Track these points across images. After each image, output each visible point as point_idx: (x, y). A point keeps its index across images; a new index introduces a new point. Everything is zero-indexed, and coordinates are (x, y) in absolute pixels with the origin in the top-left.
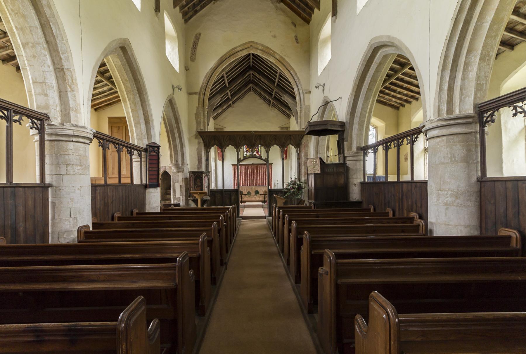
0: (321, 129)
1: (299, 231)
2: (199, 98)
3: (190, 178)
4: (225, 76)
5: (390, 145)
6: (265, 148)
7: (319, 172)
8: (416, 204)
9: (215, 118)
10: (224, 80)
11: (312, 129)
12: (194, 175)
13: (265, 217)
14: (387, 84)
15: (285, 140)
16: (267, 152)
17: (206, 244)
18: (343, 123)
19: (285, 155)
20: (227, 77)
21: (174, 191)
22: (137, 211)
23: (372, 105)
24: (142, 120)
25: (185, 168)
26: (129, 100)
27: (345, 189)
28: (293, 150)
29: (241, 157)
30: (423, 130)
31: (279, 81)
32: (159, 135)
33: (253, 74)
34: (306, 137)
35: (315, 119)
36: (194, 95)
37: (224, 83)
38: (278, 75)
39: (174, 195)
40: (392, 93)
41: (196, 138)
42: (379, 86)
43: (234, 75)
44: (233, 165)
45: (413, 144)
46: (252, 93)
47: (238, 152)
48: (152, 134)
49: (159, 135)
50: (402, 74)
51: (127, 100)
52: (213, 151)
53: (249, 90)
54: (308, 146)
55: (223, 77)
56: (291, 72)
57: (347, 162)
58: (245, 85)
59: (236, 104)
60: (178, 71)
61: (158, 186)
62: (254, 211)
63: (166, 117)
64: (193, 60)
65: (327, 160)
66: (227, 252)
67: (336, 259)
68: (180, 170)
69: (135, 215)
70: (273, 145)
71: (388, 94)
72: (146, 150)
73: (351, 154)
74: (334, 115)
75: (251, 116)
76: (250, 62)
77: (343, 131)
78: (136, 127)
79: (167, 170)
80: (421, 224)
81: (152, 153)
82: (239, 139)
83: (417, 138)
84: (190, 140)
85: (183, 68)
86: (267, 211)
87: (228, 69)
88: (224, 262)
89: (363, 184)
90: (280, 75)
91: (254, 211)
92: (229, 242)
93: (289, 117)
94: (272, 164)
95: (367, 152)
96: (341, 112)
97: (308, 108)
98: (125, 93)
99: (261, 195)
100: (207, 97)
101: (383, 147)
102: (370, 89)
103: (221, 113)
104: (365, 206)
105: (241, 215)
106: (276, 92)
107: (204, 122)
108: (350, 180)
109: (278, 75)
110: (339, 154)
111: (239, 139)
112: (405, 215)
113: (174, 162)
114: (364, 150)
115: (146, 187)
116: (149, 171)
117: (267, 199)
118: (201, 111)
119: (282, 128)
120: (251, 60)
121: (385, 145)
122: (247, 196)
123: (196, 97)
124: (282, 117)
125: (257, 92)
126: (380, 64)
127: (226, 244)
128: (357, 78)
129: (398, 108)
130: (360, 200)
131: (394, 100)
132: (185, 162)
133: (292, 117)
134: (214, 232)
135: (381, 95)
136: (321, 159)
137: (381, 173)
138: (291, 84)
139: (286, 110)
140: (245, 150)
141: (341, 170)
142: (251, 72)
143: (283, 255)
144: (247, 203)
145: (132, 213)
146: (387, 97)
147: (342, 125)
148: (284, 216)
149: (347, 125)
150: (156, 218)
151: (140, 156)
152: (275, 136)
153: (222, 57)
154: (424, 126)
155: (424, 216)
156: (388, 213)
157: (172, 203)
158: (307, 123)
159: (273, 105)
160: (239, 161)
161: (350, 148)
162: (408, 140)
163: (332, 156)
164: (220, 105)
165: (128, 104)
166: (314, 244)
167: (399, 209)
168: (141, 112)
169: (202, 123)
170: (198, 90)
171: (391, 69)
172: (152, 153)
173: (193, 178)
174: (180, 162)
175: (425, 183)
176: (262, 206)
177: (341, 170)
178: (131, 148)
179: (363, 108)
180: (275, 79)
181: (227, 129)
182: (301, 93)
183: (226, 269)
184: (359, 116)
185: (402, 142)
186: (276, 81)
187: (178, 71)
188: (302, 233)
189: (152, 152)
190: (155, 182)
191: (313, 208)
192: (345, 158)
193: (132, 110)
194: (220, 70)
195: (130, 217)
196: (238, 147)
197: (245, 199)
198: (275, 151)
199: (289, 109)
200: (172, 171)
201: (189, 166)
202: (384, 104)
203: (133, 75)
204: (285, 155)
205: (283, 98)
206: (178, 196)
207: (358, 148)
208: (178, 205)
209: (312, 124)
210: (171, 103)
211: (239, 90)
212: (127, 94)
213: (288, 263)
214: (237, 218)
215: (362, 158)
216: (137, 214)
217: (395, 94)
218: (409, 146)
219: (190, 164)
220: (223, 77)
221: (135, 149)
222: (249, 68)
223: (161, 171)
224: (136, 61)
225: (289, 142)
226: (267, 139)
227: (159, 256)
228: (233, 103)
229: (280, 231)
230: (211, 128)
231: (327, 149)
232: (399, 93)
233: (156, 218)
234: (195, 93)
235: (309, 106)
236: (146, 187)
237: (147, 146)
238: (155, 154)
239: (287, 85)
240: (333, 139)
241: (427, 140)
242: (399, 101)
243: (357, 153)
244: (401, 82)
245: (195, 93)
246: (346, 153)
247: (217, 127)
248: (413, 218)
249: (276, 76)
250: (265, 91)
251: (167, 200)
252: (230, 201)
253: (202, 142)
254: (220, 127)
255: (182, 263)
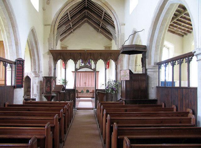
0: (132, 50)
1: (112, 122)
2: (51, 28)
3: (43, 81)
4: (69, 14)
5: (175, 62)
6: (94, 61)
7: (129, 79)
8: (191, 103)
9: (61, 40)
10: (68, 16)
11: (124, 50)
12: (46, 79)
13: (92, 109)
14: (175, 20)
15: (108, 56)
16: (95, 64)
17: (50, 129)
18: (145, 46)
19: (107, 64)
20: (70, 14)
21: (33, 89)
22: (8, 104)
23: (165, 33)
24: (14, 44)
25: (40, 74)
26: (6, 31)
27: (146, 91)
28: (113, 63)
29: (78, 67)
30: (195, 54)
31: (104, 17)
32: (24, 55)
33: (87, 12)
34: (121, 55)
35: (127, 43)
36: (48, 26)
37: (68, 18)
38: (104, 13)
39: (33, 92)
40: (179, 26)
41: (48, 54)
42: (169, 22)
43: (75, 12)
44: (72, 72)
45: (189, 63)
46: (86, 24)
47: (76, 64)
48: (20, 52)
49: (24, 55)
50: (184, 14)
51: (5, 31)
52: (60, 62)
53: (85, 22)
54: (123, 61)
55: (67, 14)
56: (112, 11)
57: (148, 73)
58: (82, 19)
59: (75, 31)
60: (38, 11)
61: (22, 87)
62: (86, 104)
63: (29, 41)
64: (48, 3)
65: (135, 71)
66: (65, 133)
67: (131, 143)
68: (37, 75)
69: (6, 107)
70: (99, 60)
71: (176, 27)
72: (15, 63)
73: (150, 68)
74: (140, 41)
75: (85, 39)
76: (85, 4)
77: (145, 52)
78: (9, 48)
79: (29, 76)
80: (192, 118)
81: (19, 65)
82: (75, 55)
83: (192, 58)
84: (44, 55)
85: (42, 8)
86: (94, 104)
87: (71, 9)
88: (63, 140)
89: (158, 88)
90: (105, 13)
91: (86, 104)
92: (69, 121)
93: (111, 40)
94: (98, 72)
95: (160, 66)
96: (144, 41)
97: (123, 35)
98: (4, 26)
99: (91, 93)
100: (56, 27)
101: (171, 63)
102: (162, 25)
103: (66, 37)
104: (159, 103)
105: (76, 107)
106: (102, 24)
107: (54, 44)
108: (150, 85)
109: (104, 13)
110: (143, 67)
111: (75, 55)
112: (184, 111)
113: (33, 70)
114: (159, 64)
115: (14, 87)
116: (17, 77)
117: (95, 96)
118: (52, 37)
119: (106, 47)
120: (86, 4)
121: (172, 62)
122: (81, 94)
123: (49, 27)
124: (106, 39)
125: (89, 23)
126: (169, 9)
127: (65, 128)
128: (154, 18)
129: (183, 36)
130: (156, 98)
131: (180, 30)
132: (40, 70)
133: (113, 40)
134: (56, 121)
135: (171, 27)
136: (130, 71)
137: (169, 79)
138: (112, 18)
139: (109, 35)
140: (81, 62)
141: (143, 78)
142: (86, 11)
143: (102, 136)
144: (81, 99)
145: (5, 105)
146: (175, 28)
147: (145, 47)
148: (103, 110)
149: (148, 48)
150: (19, 109)
151: (11, 67)
152: (101, 53)
153: (67, 2)
154: (195, 52)
155: (195, 113)
156: (173, 108)
157: (31, 98)
158: (121, 46)
159: (101, 32)
160: (76, 70)
161: (150, 64)
162: (186, 59)
163: (139, 70)
164: (65, 32)
165: (5, 33)
166: (119, 132)
167: (180, 106)
168: (13, 38)
169: (52, 44)
170: (50, 23)
171: (177, 11)
172: (19, 65)
173: (45, 82)
174: (37, 70)
175: (195, 89)
176: (91, 101)
177: (143, 78)
178: (5, 62)
179: (158, 37)
180: (102, 15)
181: (69, 49)
182: (119, 25)
183: (64, 145)
184: (155, 42)
185: (183, 61)
186: (103, 17)
187: (38, 11)
188: (113, 123)
189: (19, 64)
190: (20, 84)
191: (124, 105)
192: (146, 70)
193: (8, 37)
194: (65, 10)
195: (3, 108)
196: (75, 61)
197: (79, 95)
198: (101, 64)
199: (111, 34)
200: (32, 76)
201: (43, 73)
202: (173, 32)
203: (9, 15)
204: (107, 64)
205: (107, 27)
206: (35, 94)
207: (155, 63)
208: (35, 99)
209: (125, 47)
210: (33, 32)
211: (78, 22)
212: (5, 27)
213: (105, 143)
214: (74, 109)
215: (157, 70)
216: (8, 105)
217: (181, 27)
218: (187, 63)
219: (44, 73)
220: (67, 14)
221: (8, 63)
222: (85, 8)
223: (25, 76)
224: (11, 6)
225: (110, 57)
226: (94, 56)
227: (19, 137)
228: (74, 30)
229: (101, 119)
230: (58, 48)
231: (132, 64)
232: (183, 26)
233: (19, 109)
234: (49, 25)
235: (124, 34)
236: (14, 87)
237: (16, 60)
238: (21, 65)
239: (110, 19)
240: (140, 56)
241: (197, 61)
242: (183, 31)
243: (154, 66)
244: (184, 19)
245: (49, 25)
246: (147, 67)
247: (63, 46)
248: (189, 113)
249: (102, 14)
250: (95, 23)
251: (29, 96)
252: (70, 98)
253: (52, 57)
254: (65, 46)
255: (32, 145)
